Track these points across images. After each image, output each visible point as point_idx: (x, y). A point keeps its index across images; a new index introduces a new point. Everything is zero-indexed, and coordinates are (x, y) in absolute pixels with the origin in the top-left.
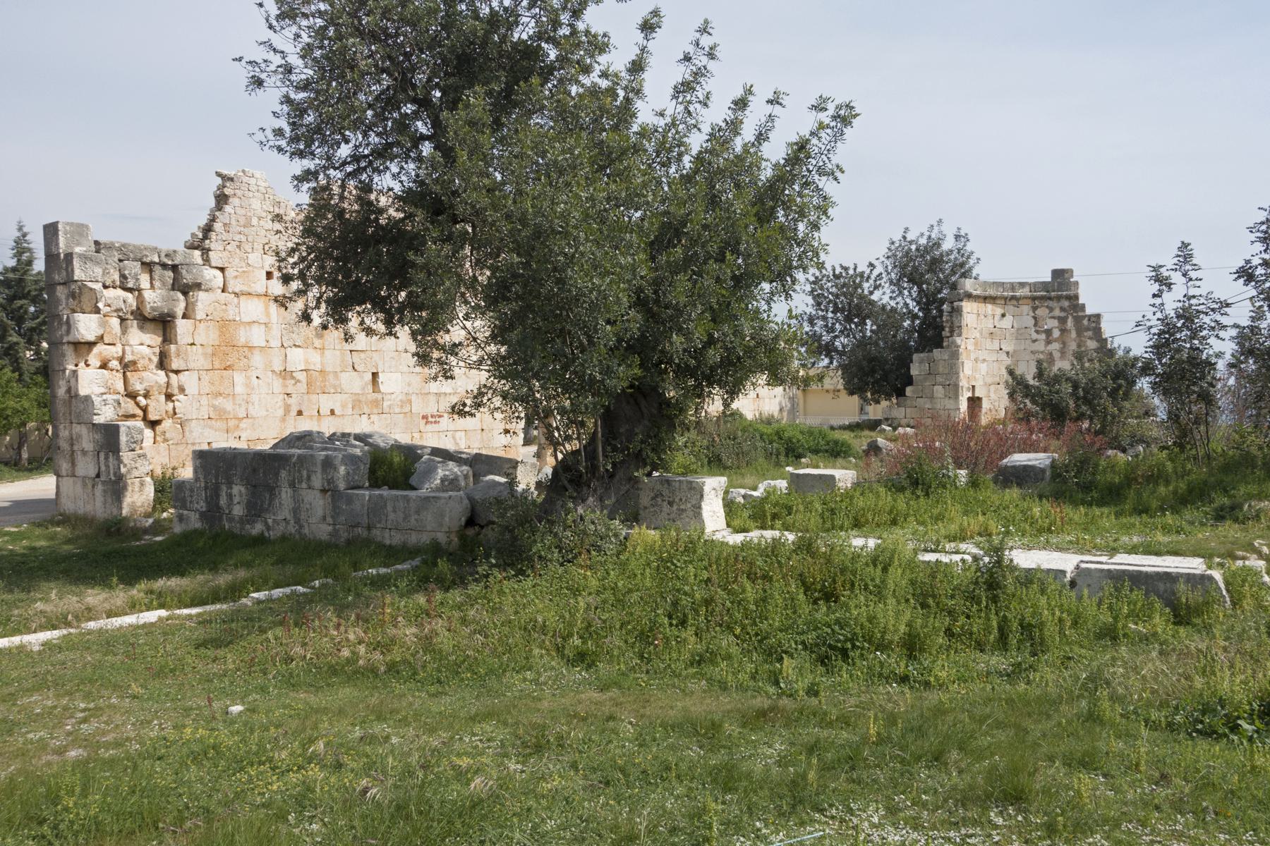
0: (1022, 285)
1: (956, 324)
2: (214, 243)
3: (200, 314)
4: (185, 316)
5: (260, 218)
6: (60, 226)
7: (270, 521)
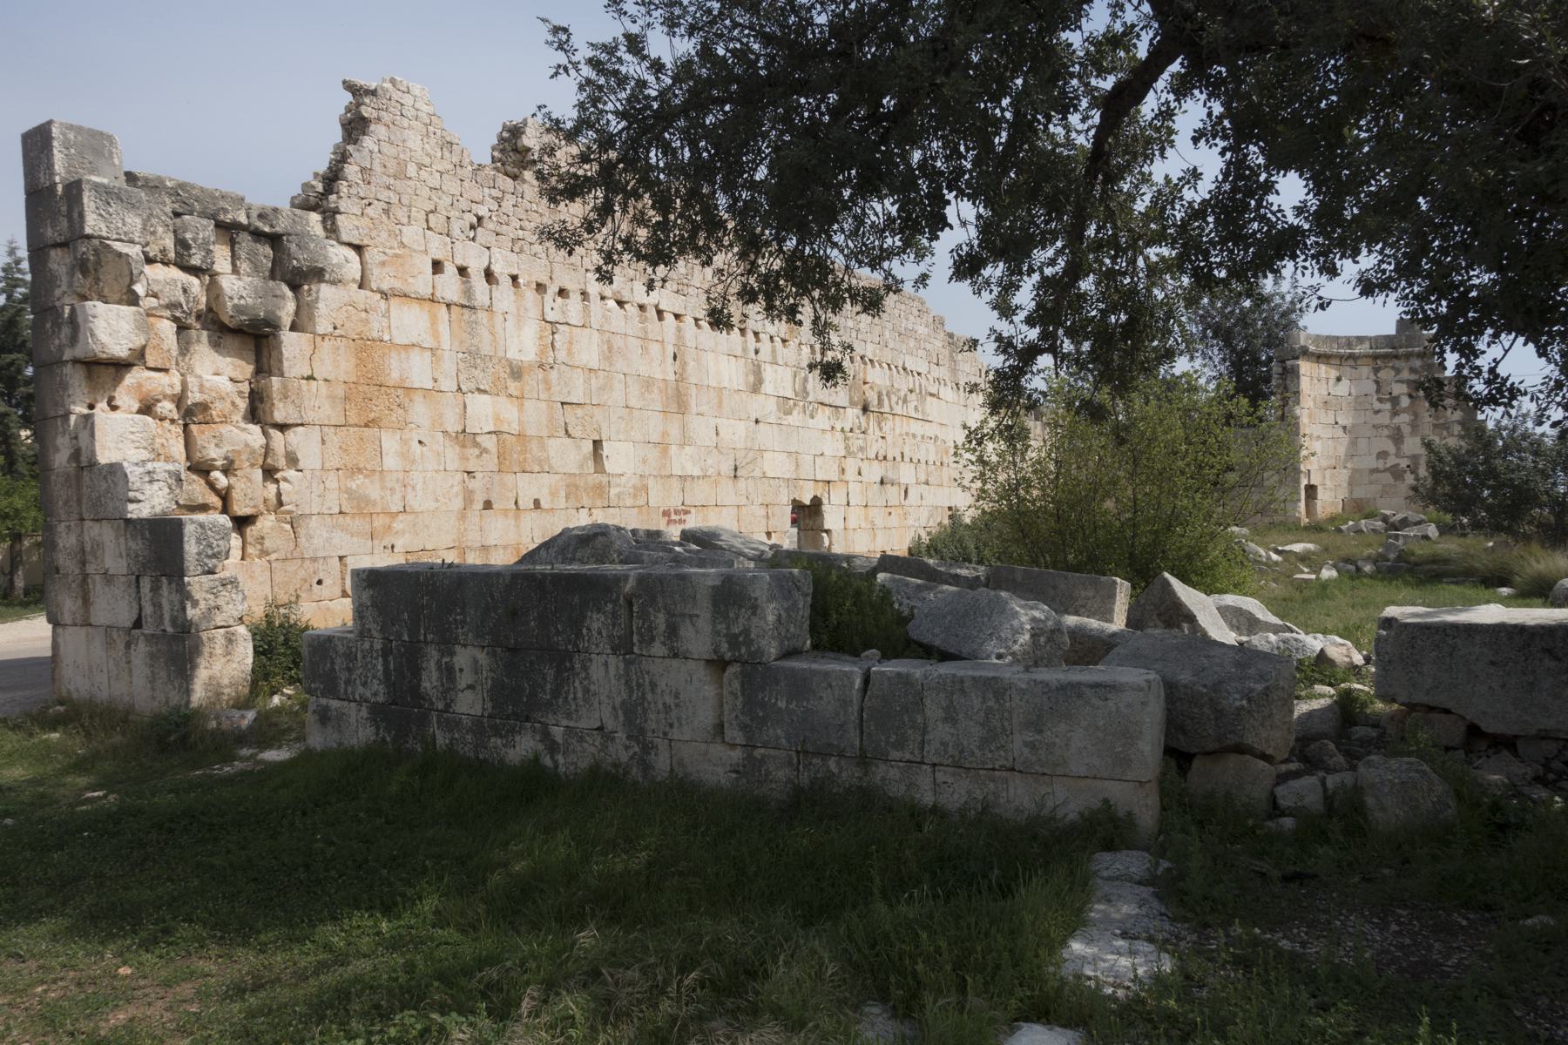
0: (1361, 339)
1: (1292, 388)
2: (345, 201)
3: (323, 326)
4: (293, 328)
5: (420, 166)
6: (55, 131)
7: (557, 732)
